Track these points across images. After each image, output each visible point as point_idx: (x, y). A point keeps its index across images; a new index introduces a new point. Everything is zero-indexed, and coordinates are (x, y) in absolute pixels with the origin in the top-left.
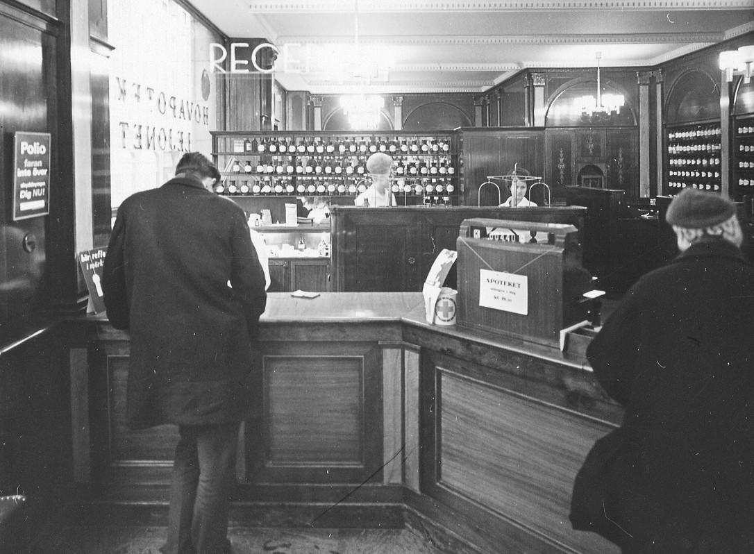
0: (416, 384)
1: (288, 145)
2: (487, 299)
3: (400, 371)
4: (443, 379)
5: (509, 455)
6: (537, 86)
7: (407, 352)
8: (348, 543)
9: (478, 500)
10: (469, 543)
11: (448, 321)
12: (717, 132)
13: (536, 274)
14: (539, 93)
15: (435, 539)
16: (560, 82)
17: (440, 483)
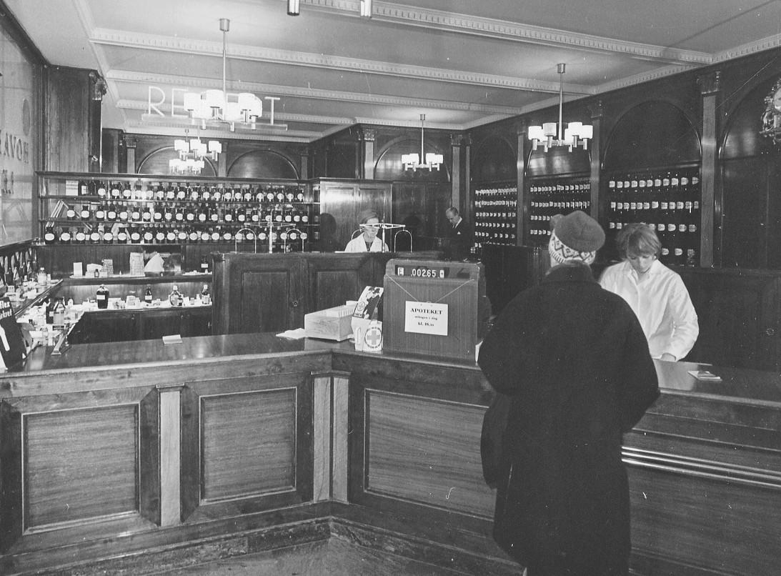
0: (346, 407)
1: (255, 192)
2: (411, 325)
3: (330, 398)
4: (371, 398)
5: (432, 453)
6: (368, 141)
7: (335, 379)
8: (284, 559)
9: (404, 496)
10: (395, 532)
11: (376, 347)
12: (514, 190)
13: (455, 301)
14: (369, 148)
15: (361, 539)
16: (388, 139)
17: (368, 490)
